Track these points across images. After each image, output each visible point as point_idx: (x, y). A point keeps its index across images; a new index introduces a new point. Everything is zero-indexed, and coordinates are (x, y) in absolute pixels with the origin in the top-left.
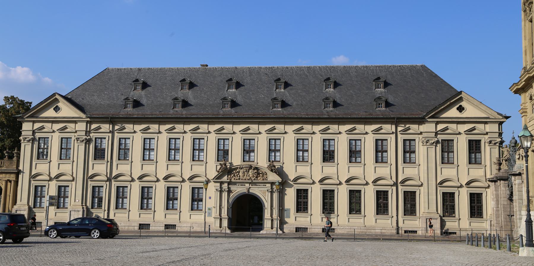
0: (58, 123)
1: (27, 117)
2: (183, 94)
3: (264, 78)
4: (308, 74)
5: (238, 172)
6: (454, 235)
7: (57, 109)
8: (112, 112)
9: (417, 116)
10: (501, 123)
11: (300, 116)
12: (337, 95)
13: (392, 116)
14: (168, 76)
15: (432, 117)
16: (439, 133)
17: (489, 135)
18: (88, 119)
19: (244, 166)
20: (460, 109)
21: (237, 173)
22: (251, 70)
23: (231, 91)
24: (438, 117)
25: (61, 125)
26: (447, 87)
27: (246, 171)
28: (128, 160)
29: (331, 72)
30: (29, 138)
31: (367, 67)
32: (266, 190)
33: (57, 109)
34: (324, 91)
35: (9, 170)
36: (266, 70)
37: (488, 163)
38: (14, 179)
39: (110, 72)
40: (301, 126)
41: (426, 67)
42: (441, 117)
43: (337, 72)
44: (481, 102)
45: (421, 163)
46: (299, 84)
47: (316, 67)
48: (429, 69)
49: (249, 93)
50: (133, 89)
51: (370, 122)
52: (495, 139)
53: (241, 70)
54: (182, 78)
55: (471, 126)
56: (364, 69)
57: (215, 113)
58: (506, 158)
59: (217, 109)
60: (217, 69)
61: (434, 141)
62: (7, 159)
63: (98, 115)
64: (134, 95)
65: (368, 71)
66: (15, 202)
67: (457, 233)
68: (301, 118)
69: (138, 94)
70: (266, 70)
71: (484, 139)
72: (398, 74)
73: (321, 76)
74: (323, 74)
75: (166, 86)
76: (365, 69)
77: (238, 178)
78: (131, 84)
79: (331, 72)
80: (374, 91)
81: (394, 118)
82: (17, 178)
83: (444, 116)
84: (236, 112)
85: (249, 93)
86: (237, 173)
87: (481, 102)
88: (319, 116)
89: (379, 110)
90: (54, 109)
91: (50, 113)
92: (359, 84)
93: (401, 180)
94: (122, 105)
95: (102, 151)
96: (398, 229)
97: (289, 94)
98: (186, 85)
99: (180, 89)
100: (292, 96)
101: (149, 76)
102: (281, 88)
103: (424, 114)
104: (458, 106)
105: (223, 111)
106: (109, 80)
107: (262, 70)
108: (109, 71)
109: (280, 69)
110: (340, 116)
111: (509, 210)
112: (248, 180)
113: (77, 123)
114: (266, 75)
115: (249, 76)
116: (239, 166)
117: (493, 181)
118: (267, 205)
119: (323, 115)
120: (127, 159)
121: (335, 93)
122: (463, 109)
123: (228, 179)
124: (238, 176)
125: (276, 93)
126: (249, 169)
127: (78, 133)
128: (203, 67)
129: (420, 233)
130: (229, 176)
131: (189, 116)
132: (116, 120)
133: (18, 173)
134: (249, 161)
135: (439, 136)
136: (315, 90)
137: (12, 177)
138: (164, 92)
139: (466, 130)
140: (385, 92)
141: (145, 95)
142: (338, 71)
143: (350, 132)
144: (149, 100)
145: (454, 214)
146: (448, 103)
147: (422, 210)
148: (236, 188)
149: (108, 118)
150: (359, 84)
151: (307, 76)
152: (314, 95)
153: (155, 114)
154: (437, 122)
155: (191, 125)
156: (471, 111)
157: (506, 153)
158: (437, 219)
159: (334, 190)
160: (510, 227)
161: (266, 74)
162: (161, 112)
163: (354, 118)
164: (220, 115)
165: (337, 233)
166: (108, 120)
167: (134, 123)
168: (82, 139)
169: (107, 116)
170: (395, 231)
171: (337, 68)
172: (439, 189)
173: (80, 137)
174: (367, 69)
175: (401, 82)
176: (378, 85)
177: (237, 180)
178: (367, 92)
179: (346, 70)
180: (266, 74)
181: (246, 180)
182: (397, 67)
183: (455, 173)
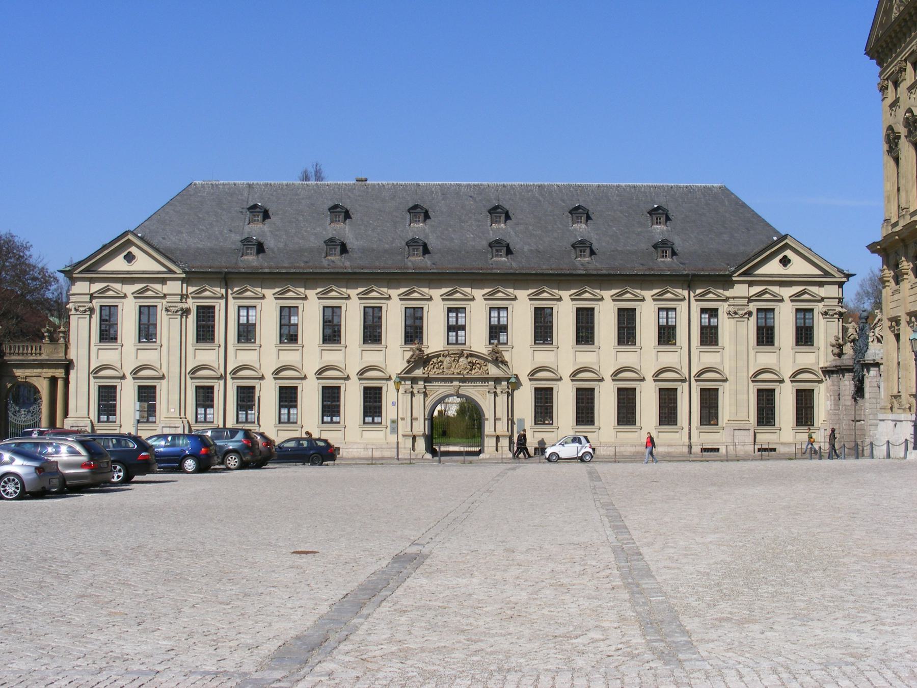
0: (791, 286)
1: (80, 272)
2: (335, 230)
3: (468, 203)
4: (541, 199)
5: (440, 361)
6: (716, 453)
7: (130, 258)
8: (222, 263)
9: (721, 273)
10: (841, 285)
11: (539, 271)
12: (592, 234)
13: (685, 272)
14: (303, 199)
15: (745, 274)
16: (753, 298)
17: (827, 302)
18: (184, 276)
19: (450, 352)
20: (785, 261)
21: (440, 364)
22: (444, 191)
23: (416, 226)
24: (94, 271)
25: (138, 286)
26: (762, 224)
27: (454, 361)
28: (155, 342)
29: (577, 195)
30: (84, 306)
31: (634, 187)
32: (488, 390)
33: (130, 258)
34: (570, 228)
35: (54, 360)
36: (470, 190)
37: (822, 349)
38: (63, 375)
39: (200, 190)
40: (145, 285)
41: (728, 190)
42: (100, 270)
43: (588, 195)
44: (810, 249)
45: (726, 345)
46: (528, 216)
47: (552, 186)
48: (732, 194)
49: (447, 230)
50: (247, 223)
51: (568, 280)
52: (834, 308)
53: (427, 189)
54: (331, 204)
55: (800, 288)
56: (630, 190)
57: (553, 266)
58: (852, 337)
59: (399, 257)
60: (386, 187)
61: (746, 311)
62: (49, 342)
63: (203, 267)
64: (251, 232)
65: (637, 195)
66: (66, 414)
67: (720, 450)
68: (543, 274)
69: (257, 229)
70: (470, 190)
71: (161, 304)
72: (686, 200)
73: (563, 201)
74: (565, 197)
75: (303, 215)
76: (633, 190)
77: (441, 371)
78: (241, 212)
79: (577, 195)
80: (650, 229)
81: (687, 275)
82: (67, 373)
83: (102, 269)
84: (434, 264)
85: (447, 230)
86: (440, 364)
87: (810, 249)
88: (571, 272)
89: (662, 261)
90: (125, 257)
91: (118, 264)
92: (626, 216)
93: (231, 369)
94: (235, 249)
95: (209, 328)
96: (690, 447)
97: (515, 233)
98: (258, 216)
99: (329, 222)
100: (520, 236)
101: (269, 198)
102: (500, 222)
103: (733, 269)
104: (125, 253)
105: (410, 261)
106: (201, 205)
107: (463, 190)
108: (196, 188)
109: (493, 188)
110: (604, 272)
111: (853, 413)
112: (458, 374)
113: (166, 284)
114: (471, 199)
115: (443, 199)
116: (442, 353)
117: (827, 372)
118: (488, 413)
119: (575, 269)
120: (154, 340)
121: (589, 232)
122: (789, 261)
123: (423, 373)
124: (442, 367)
125: (492, 230)
126: (459, 357)
127: (169, 298)
128: (360, 182)
129: (723, 450)
130: (426, 369)
131: (358, 271)
132: (234, 276)
133: (68, 366)
134: (457, 343)
135: (94, 301)
136: (556, 226)
137: (59, 373)
138: (302, 228)
139: (793, 294)
140: (668, 231)
141: (271, 232)
142: (590, 193)
143: (139, 295)
144: (280, 242)
145: (379, 416)
146: (768, 252)
147: (726, 418)
148: (437, 387)
149: (220, 273)
150: (626, 216)
151: (539, 201)
152: (555, 235)
153: (299, 267)
154: (751, 281)
155: (793, 287)
156: (798, 267)
157: (851, 331)
158: (749, 430)
159: (594, 389)
160: (854, 437)
161: (471, 197)
162: (307, 262)
163: (626, 275)
164: (408, 268)
165: (600, 454)
166: (219, 276)
167: (187, 281)
168: (84, 309)
169: (218, 270)
170: (686, 449)
171: (587, 189)
172: (92, 380)
173: (173, 305)
174: (635, 190)
175: (690, 214)
176: (657, 219)
177: (438, 374)
178: (639, 230)
179: (602, 192)
180: (471, 197)
181: (453, 374)
182: (683, 188)
183: (257, 358)
